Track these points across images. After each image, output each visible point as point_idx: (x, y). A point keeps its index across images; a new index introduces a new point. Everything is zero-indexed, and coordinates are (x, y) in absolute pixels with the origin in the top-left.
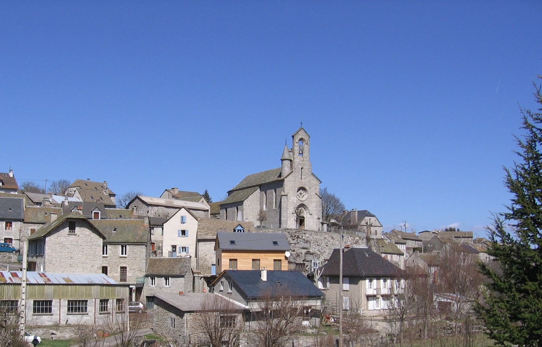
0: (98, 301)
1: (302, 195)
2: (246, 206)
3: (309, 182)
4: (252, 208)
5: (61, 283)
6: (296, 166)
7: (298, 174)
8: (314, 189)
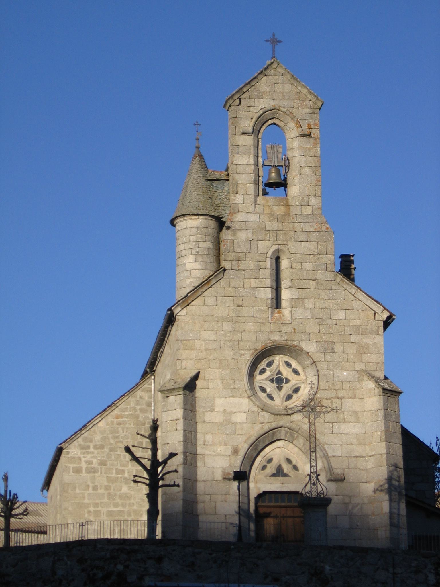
0: (231, 181)
1: (287, 388)
2: (78, 471)
3: (321, 321)
4: (110, 480)
5: (196, 286)
6: (241, 248)
7: (254, 283)
8: (352, 350)
